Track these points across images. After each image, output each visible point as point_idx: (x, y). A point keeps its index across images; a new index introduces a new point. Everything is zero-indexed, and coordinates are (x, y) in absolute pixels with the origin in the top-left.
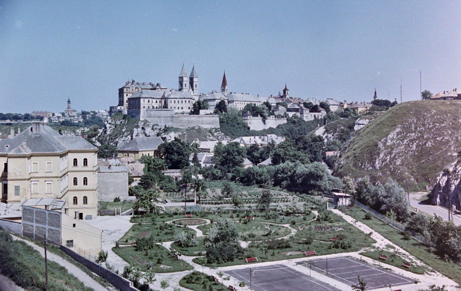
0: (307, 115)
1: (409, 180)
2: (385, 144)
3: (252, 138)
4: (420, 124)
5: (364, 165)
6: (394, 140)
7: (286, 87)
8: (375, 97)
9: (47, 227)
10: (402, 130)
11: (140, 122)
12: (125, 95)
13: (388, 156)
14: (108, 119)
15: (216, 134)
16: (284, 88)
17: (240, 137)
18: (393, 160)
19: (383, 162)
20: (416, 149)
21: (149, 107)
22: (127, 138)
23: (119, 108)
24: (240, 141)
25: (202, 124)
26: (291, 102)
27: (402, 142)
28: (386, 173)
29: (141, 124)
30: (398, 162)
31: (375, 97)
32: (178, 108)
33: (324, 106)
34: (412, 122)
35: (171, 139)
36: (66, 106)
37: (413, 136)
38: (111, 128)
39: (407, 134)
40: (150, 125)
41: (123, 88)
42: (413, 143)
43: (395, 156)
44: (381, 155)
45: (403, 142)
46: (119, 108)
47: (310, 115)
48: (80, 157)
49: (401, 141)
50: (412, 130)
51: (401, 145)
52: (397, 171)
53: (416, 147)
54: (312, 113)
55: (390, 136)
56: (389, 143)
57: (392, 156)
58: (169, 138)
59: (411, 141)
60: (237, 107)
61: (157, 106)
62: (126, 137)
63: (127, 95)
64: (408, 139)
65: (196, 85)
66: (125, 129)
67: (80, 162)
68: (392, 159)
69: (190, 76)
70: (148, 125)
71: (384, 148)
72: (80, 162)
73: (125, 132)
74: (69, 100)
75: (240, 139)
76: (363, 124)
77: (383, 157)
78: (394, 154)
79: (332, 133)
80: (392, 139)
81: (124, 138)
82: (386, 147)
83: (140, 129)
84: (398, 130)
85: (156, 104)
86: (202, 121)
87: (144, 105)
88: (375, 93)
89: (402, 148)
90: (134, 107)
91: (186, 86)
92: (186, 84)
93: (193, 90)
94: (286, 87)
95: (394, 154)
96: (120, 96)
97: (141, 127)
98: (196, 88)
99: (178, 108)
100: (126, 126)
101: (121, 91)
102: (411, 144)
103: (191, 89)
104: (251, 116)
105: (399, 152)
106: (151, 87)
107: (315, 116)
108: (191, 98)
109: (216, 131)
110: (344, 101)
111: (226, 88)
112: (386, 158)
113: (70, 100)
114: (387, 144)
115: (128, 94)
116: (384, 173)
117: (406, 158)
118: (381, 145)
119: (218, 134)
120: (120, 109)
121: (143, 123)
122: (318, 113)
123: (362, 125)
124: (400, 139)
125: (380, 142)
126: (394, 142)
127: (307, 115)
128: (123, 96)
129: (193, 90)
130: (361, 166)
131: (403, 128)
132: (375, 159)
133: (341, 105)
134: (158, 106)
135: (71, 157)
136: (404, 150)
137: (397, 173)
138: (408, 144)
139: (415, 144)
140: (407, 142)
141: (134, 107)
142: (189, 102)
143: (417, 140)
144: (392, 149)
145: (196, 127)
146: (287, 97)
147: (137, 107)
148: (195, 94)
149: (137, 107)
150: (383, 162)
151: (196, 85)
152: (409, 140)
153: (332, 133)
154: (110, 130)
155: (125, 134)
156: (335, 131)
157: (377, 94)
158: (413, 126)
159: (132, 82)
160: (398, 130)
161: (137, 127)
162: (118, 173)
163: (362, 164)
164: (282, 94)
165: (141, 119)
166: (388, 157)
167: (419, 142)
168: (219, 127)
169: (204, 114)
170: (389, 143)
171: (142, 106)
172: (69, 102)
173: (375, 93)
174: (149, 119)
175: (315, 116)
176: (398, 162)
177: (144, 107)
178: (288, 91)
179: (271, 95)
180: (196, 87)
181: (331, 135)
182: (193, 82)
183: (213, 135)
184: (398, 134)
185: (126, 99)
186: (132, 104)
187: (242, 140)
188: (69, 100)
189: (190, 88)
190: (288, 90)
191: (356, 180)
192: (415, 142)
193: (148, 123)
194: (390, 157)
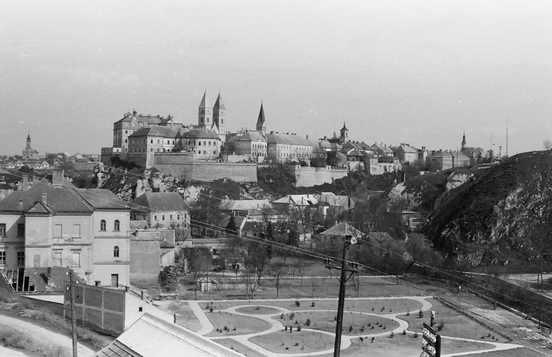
0: (374, 166)
1: (535, 257)
2: (502, 208)
3: (305, 196)
4: (548, 181)
5: (476, 236)
6: (515, 204)
7: (344, 125)
8: (464, 142)
9: (103, 310)
10: (525, 190)
11: (147, 171)
12: (124, 131)
13: (507, 225)
14: (100, 166)
15: (251, 191)
16: (342, 127)
17: (288, 196)
18: (514, 231)
19: (500, 233)
20: (542, 216)
21: (158, 150)
22: (127, 194)
23: (115, 150)
24: (289, 202)
25: (233, 175)
26: (353, 147)
27: (525, 207)
28: (504, 248)
29: (147, 174)
30: (521, 234)
31: (464, 142)
32: (200, 153)
33: (398, 153)
34: (537, 180)
35: (190, 196)
36: (24, 145)
37: (539, 198)
38: (104, 179)
39: (531, 195)
40: (159, 176)
41: (121, 121)
42: (539, 208)
43: (516, 225)
44: (498, 224)
45: (527, 206)
46: (115, 150)
47: (379, 165)
48: (110, 217)
49: (524, 205)
50: (537, 190)
51: (524, 210)
52: (519, 245)
53: (543, 213)
54: (381, 164)
55: (510, 198)
56: (509, 207)
57: (513, 225)
58: (188, 195)
59: (537, 205)
60: (281, 152)
61: (169, 148)
62: (127, 191)
63: (126, 132)
64: (533, 202)
65: (222, 120)
66: (125, 180)
67: (110, 226)
68: (513, 230)
69: (200, 106)
70: (157, 176)
71: (501, 213)
72: (110, 226)
73: (124, 185)
74: (29, 136)
75: (288, 198)
76: (458, 181)
77: (501, 226)
78: (514, 223)
79: (414, 193)
80: (512, 202)
81: (123, 193)
82: (505, 213)
83: (145, 181)
84: (519, 190)
85: (169, 145)
86: (233, 172)
87: (153, 147)
88: (464, 137)
89: (525, 214)
90: (138, 150)
91: (208, 121)
92: (208, 119)
93: (218, 126)
94: (344, 125)
95: (514, 223)
96: (115, 134)
97: (147, 178)
98: (222, 125)
99: (200, 153)
100: (125, 176)
101: (118, 126)
102: (536, 210)
103: (215, 125)
104: (300, 166)
105: (521, 219)
106: (159, 121)
107: (385, 169)
108: (217, 139)
109: (252, 186)
110: (423, 147)
111: (264, 125)
112: (504, 228)
113: (30, 137)
114: (506, 208)
115: (128, 131)
116: (502, 248)
117: (530, 228)
118: (497, 209)
119: (256, 190)
120: (116, 151)
121: (149, 173)
122: (389, 164)
123: (456, 182)
124: (521, 202)
125: (496, 206)
126: (515, 206)
127: (374, 166)
128: (121, 134)
129: (218, 126)
130: (471, 238)
131: (526, 188)
132: (491, 228)
133: (420, 153)
134: (171, 149)
135: (98, 216)
136: (527, 217)
137: (520, 247)
138: (533, 209)
139: (541, 209)
140: (532, 206)
141: (138, 150)
142: (215, 144)
143: (543, 204)
144: (512, 216)
145: (225, 180)
146: (346, 139)
147: (142, 150)
148: (221, 132)
149: (142, 150)
150: (500, 233)
151: (222, 120)
152: (534, 204)
153: (414, 193)
154: (102, 181)
155: (125, 188)
156: (418, 189)
157: (466, 140)
158: (538, 185)
159: (132, 113)
160: (519, 190)
161: (142, 178)
162: (149, 242)
163: (472, 235)
164: (338, 135)
165: (148, 166)
166: (507, 227)
167: (547, 206)
168: (256, 180)
169: (236, 161)
170: (509, 207)
171: (149, 148)
172: (29, 139)
173: (464, 137)
174: (158, 167)
175: (385, 169)
176: (521, 234)
177: (152, 150)
178: (347, 132)
179: (325, 137)
180: (222, 123)
181: (413, 195)
182: (218, 115)
183: (247, 191)
184: (520, 195)
185: (125, 137)
186: (134, 145)
187: (291, 199)
188: (29, 136)
189: (213, 124)
190: (347, 130)
191: (464, 257)
192: (542, 207)
193: (157, 173)
194: (510, 226)
